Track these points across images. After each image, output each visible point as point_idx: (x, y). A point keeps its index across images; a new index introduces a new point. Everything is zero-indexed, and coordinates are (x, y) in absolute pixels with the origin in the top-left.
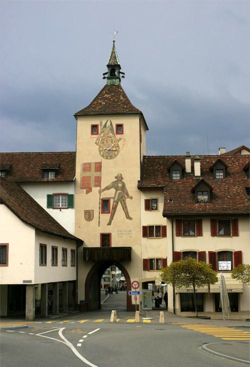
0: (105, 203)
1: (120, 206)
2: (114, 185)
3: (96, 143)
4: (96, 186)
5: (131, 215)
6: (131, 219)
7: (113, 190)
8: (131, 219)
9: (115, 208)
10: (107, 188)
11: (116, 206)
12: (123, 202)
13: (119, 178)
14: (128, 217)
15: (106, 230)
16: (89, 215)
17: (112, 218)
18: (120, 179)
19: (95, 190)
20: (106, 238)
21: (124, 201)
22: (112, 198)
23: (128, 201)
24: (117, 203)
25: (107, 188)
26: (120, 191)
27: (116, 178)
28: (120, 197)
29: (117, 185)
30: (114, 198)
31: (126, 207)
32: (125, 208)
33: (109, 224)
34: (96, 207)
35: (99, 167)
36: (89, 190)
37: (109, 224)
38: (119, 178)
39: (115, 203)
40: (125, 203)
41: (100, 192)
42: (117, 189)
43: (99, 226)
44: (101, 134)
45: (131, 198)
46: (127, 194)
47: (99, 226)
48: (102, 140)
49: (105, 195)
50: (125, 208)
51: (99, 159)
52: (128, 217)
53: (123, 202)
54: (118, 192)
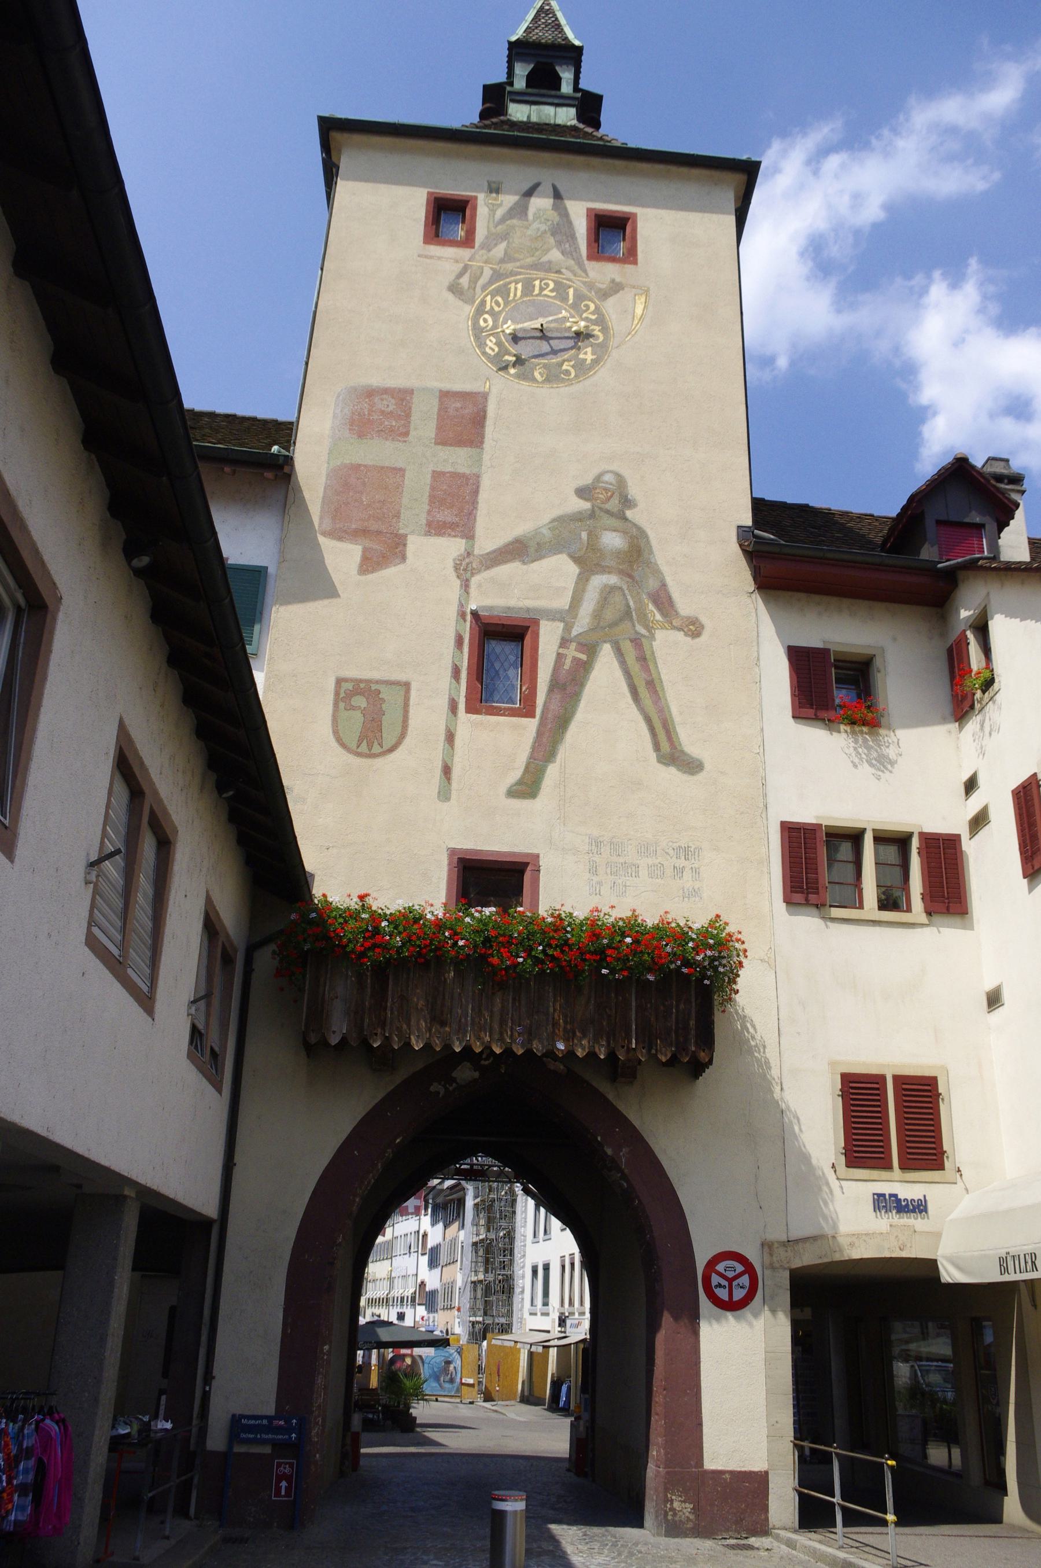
0: (498, 642)
1: (606, 674)
3: (454, 288)
4: (436, 528)
5: (690, 742)
6: (691, 766)
8: (691, 766)
9: (570, 684)
10: (518, 550)
11: (582, 669)
12: (627, 647)
13: (607, 500)
14: (672, 754)
15: (497, 841)
18: (614, 505)
19: (432, 555)
21: (637, 642)
22: (554, 615)
23: (667, 645)
24: (591, 650)
25: (518, 550)
26: (613, 579)
27: (582, 492)
28: (609, 615)
30: (567, 617)
31: (653, 686)
32: (645, 687)
33: (527, 787)
35: (465, 421)
36: (385, 550)
37: (527, 787)
38: (607, 500)
39: (572, 652)
42: (589, 562)
43: (444, 795)
44: (487, 246)
45: (694, 628)
46: (663, 601)
47: (444, 795)
48: (497, 276)
49: (503, 592)
50: (645, 687)
51: (472, 373)
52: (672, 754)
53: (627, 647)
54: (598, 581)
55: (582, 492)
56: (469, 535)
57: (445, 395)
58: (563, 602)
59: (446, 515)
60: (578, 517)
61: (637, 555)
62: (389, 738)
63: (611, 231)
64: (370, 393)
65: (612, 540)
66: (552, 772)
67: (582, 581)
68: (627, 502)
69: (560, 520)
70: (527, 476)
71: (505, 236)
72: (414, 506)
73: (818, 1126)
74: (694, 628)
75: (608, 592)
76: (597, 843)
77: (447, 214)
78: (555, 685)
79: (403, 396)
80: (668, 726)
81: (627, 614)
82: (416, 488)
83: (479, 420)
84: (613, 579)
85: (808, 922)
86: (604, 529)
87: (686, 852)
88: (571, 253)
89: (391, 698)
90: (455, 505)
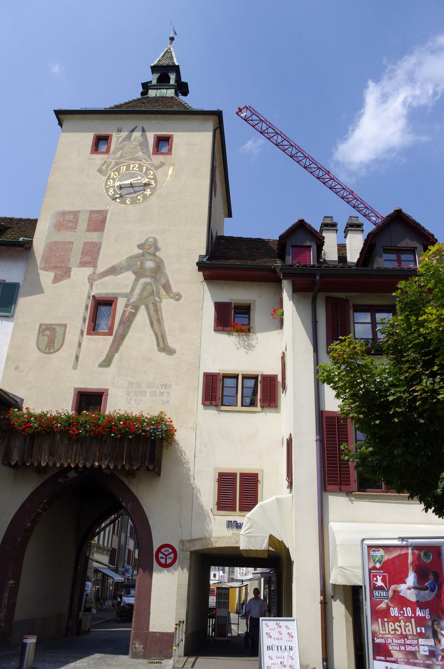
0: (102, 305)
1: (142, 317)
2: (135, 265)
4: (83, 264)
5: (171, 342)
6: (170, 351)
7: (128, 277)
8: (170, 351)
9: (127, 322)
10: (113, 271)
11: (133, 315)
12: (151, 306)
13: (150, 249)
14: (164, 347)
15: (92, 385)
16: (50, 338)
17: (115, 348)
18: (152, 250)
19: (80, 274)
20: (89, 400)
21: (155, 304)
23: (167, 305)
24: (136, 308)
25: (113, 271)
26: (148, 280)
27: (140, 246)
28: (145, 294)
29: (142, 263)
30: (128, 296)
31: (159, 321)
32: (156, 322)
34: (75, 313)
35: (98, 221)
36: (63, 273)
38: (150, 249)
39: (129, 309)
40: (157, 311)
41: (91, 280)
42: (139, 274)
43: (75, 367)
44: (114, 153)
45: (178, 297)
46: (167, 287)
49: (103, 289)
50: (156, 322)
52: (164, 347)
54: (142, 281)
55: (140, 246)
56: (95, 266)
57: (92, 212)
58: (128, 290)
59: (87, 259)
60: (137, 256)
61: (159, 268)
62: (56, 347)
63: (163, 142)
64: (64, 213)
65: (150, 264)
66: (117, 356)
67: (136, 281)
68: (157, 249)
69: (131, 258)
70: (117, 247)
71: (122, 148)
72: (76, 255)
73: (265, 648)
74: (178, 297)
75: (146, 285)
76: (131, 383)
77: (101, 141)
78: (122, 322)
79: (76, 214)
80: (163, 337)
81: (152, 293)
82: (78, 248)
83: (103, 221)
84: (148, 280)
85: (212, 413)
86: (148, 263)
87: (166, 386)
88: (146, 152)
89: (59, 330)
90: (91, 254)
